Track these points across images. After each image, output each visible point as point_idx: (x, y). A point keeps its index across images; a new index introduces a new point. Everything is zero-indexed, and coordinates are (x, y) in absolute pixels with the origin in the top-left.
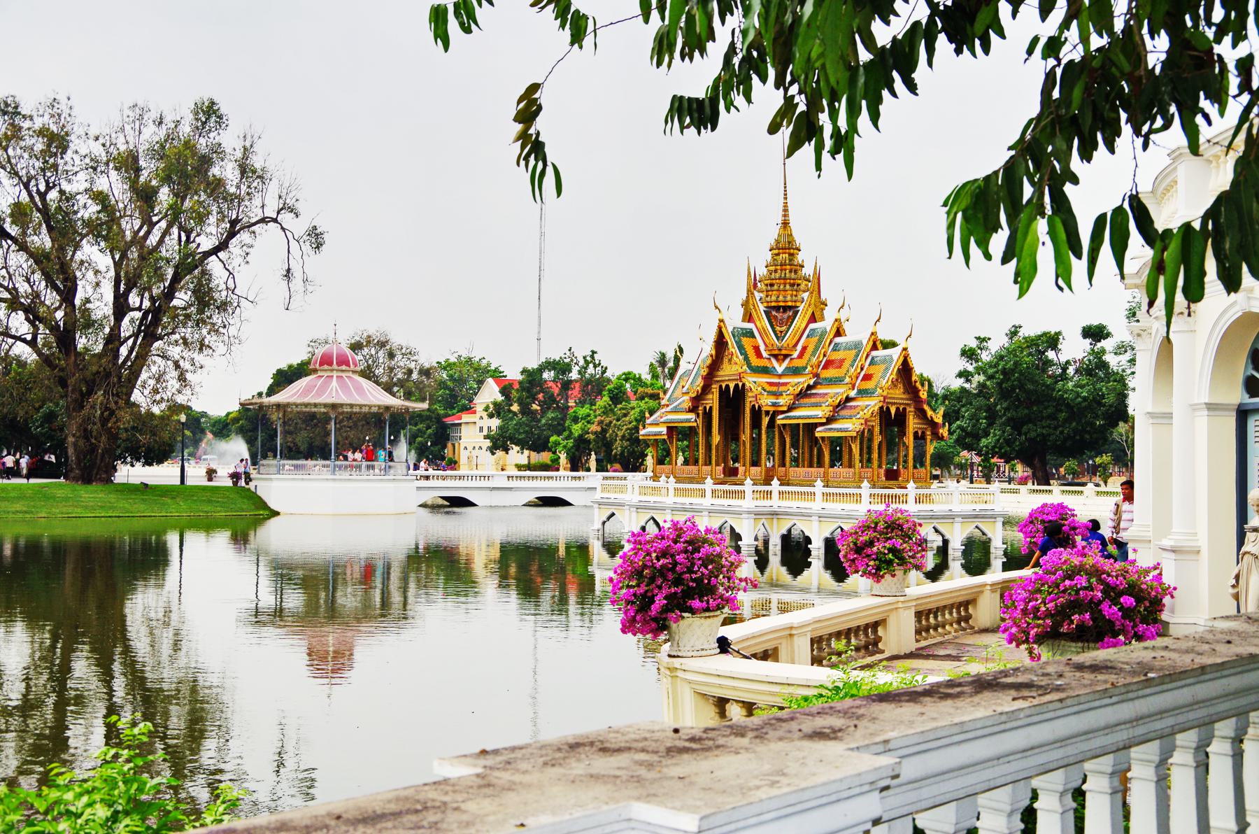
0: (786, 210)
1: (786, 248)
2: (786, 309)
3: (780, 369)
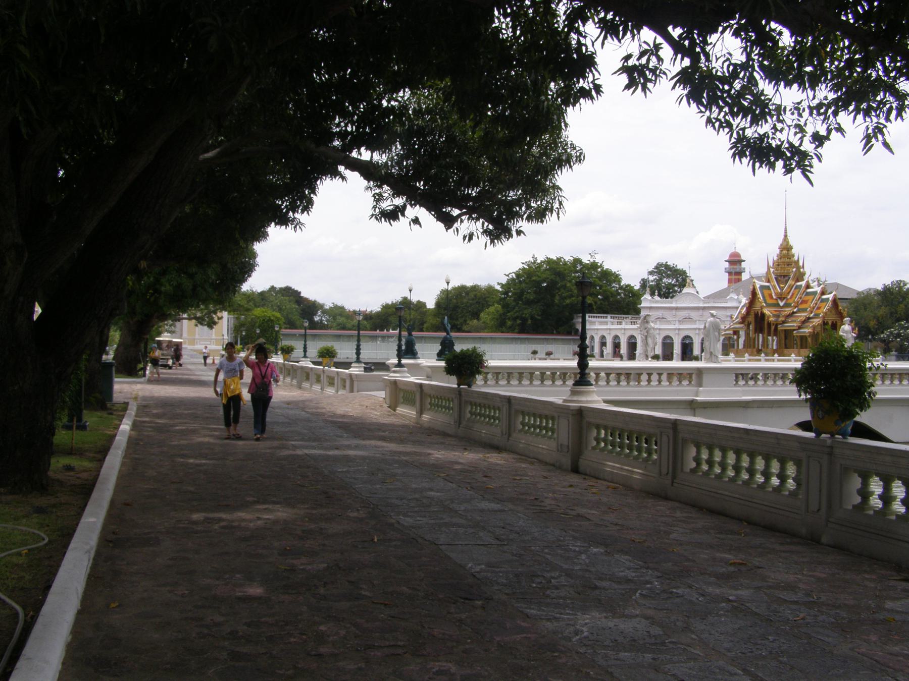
0: (786, 230)
1: (786, 248)
2: (785, 276)
3: (781, 304)
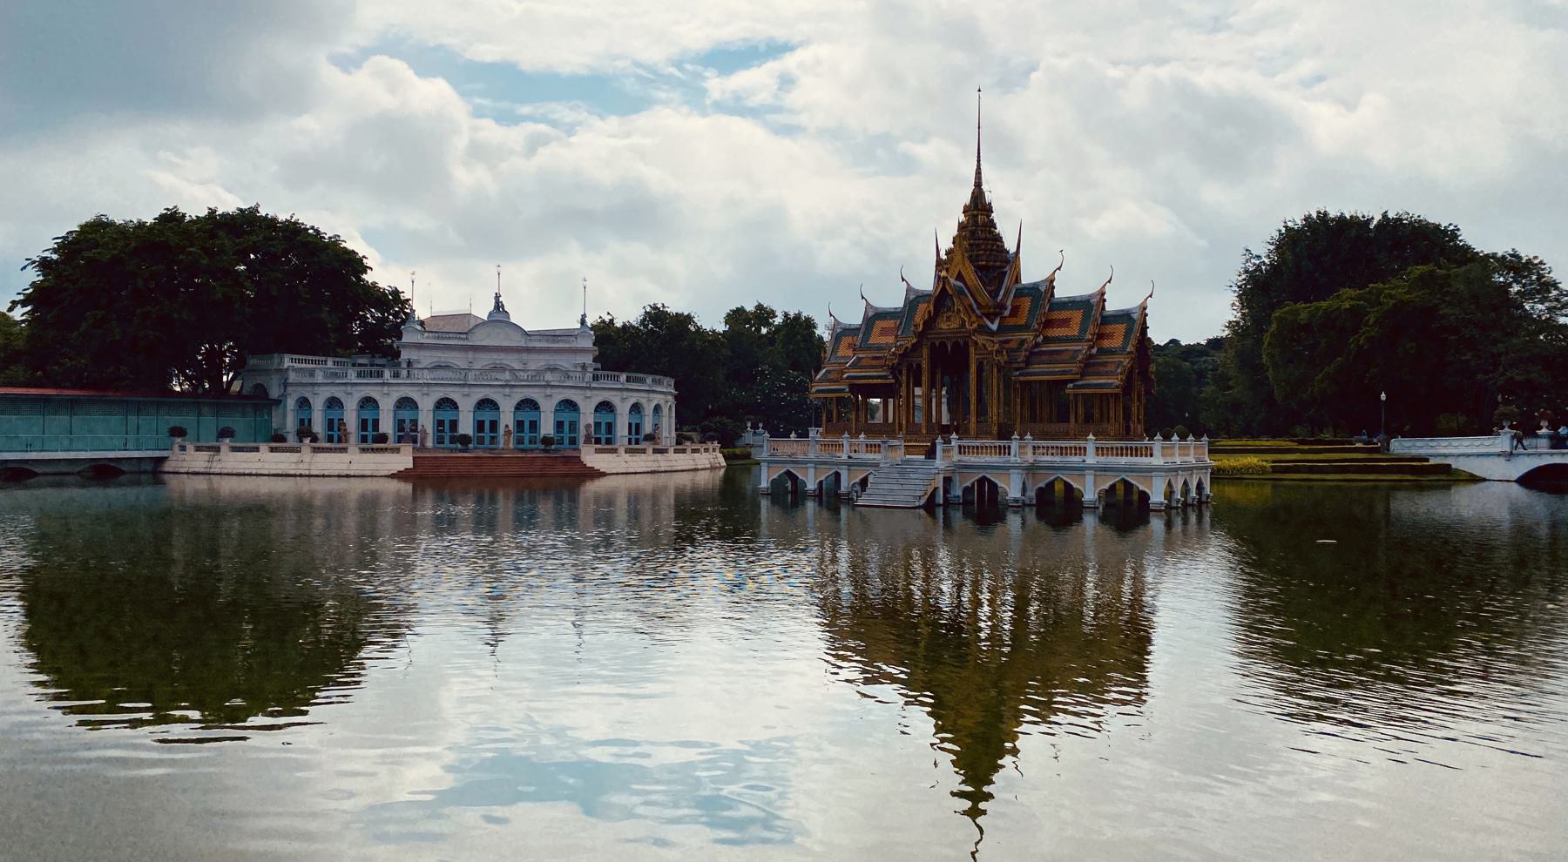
0: (672, 744)
3: (994, 327)
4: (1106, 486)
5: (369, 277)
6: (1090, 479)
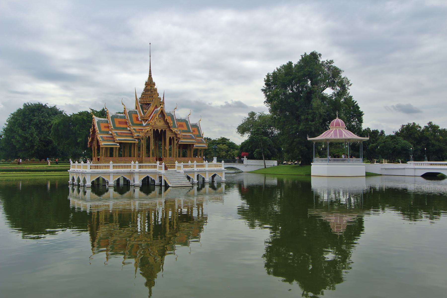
0: (150, 70)
3: (144, 124)
4: (117, 179)
5: (440, 128)
6: (111, 177)
